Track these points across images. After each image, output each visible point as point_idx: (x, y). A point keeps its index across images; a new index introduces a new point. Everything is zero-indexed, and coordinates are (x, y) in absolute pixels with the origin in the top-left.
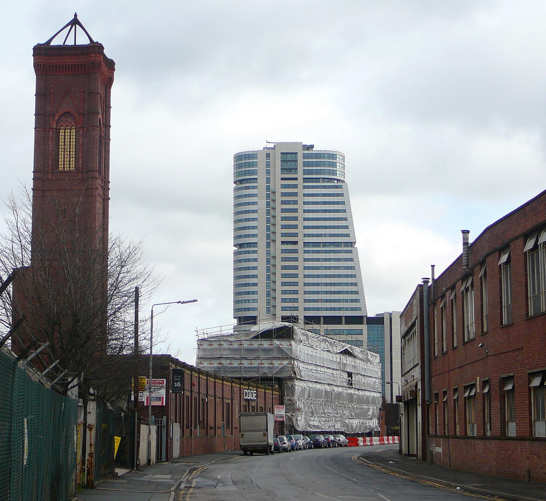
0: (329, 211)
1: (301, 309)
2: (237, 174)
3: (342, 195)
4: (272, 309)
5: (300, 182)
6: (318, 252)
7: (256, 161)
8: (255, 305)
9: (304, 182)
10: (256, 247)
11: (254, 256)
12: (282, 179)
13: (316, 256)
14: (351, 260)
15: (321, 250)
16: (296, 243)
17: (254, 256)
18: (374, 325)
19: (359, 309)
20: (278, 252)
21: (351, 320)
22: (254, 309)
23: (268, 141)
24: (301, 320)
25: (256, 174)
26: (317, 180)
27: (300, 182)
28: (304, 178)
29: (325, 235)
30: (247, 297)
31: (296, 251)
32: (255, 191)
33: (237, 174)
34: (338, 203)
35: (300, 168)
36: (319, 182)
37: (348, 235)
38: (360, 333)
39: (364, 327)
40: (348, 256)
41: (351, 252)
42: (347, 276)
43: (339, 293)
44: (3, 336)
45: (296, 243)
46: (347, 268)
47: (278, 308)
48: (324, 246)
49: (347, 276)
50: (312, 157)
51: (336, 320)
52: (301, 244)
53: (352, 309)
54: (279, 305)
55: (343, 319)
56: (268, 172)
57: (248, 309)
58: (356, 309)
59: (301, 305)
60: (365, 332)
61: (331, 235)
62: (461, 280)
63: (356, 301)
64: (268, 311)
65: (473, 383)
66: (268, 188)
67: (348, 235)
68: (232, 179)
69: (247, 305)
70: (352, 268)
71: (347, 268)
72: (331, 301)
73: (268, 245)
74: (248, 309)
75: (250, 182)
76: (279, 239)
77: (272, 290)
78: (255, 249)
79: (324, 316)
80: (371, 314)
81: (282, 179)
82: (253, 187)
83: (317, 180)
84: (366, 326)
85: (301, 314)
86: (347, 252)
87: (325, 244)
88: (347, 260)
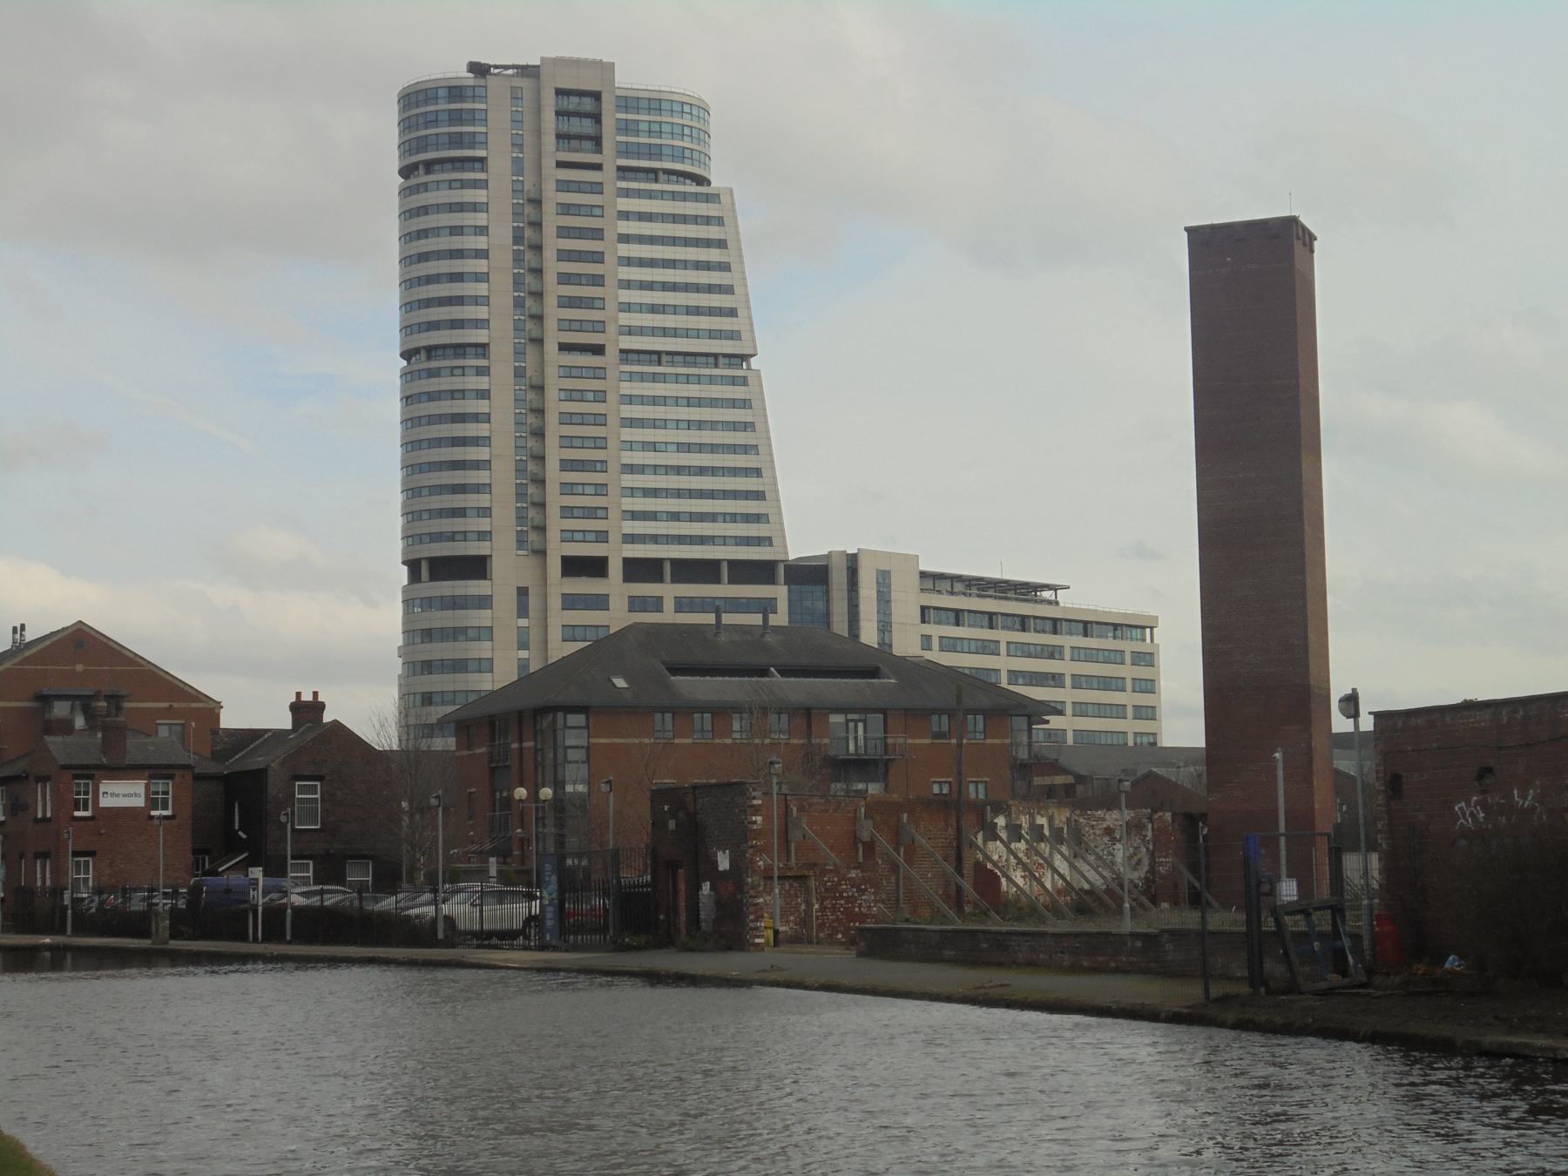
0: (714, 471)
2: (407, 147)
3: (728, 290)
9: (619, 178)
12: (560, 165)
13: (659, 389)
17: (479, 195)
24: (615, 569)
26: (653, 174)
27: (607, 176)
28: (620, 169)
29: (675, 310)
32: (479, 195)
33: (408, 146)
34: (707, 243)
37: (734, 335)
40: (737, 392)
41: (744, 381)
45: (598, 350)
46: (734, 426)
47: (553, 535)
54: (555, 524)
61: (689, 402)
63: (757, 518)
64: (521, 542)
67: (734, 335)
68: (394, 164)
70: (747, 426)
71: (734, 426)
72: (651, 263)
73: (519, 353)
76: (553, 338)
77: (532, 481)
78: (482, 362)
80: (799, 546)
81: (560, 165)
82: (475, 184)
83: (653, 174)
84: (786, 587)
85: (617, 553)
86: (734, 381)
88: (733, 403)
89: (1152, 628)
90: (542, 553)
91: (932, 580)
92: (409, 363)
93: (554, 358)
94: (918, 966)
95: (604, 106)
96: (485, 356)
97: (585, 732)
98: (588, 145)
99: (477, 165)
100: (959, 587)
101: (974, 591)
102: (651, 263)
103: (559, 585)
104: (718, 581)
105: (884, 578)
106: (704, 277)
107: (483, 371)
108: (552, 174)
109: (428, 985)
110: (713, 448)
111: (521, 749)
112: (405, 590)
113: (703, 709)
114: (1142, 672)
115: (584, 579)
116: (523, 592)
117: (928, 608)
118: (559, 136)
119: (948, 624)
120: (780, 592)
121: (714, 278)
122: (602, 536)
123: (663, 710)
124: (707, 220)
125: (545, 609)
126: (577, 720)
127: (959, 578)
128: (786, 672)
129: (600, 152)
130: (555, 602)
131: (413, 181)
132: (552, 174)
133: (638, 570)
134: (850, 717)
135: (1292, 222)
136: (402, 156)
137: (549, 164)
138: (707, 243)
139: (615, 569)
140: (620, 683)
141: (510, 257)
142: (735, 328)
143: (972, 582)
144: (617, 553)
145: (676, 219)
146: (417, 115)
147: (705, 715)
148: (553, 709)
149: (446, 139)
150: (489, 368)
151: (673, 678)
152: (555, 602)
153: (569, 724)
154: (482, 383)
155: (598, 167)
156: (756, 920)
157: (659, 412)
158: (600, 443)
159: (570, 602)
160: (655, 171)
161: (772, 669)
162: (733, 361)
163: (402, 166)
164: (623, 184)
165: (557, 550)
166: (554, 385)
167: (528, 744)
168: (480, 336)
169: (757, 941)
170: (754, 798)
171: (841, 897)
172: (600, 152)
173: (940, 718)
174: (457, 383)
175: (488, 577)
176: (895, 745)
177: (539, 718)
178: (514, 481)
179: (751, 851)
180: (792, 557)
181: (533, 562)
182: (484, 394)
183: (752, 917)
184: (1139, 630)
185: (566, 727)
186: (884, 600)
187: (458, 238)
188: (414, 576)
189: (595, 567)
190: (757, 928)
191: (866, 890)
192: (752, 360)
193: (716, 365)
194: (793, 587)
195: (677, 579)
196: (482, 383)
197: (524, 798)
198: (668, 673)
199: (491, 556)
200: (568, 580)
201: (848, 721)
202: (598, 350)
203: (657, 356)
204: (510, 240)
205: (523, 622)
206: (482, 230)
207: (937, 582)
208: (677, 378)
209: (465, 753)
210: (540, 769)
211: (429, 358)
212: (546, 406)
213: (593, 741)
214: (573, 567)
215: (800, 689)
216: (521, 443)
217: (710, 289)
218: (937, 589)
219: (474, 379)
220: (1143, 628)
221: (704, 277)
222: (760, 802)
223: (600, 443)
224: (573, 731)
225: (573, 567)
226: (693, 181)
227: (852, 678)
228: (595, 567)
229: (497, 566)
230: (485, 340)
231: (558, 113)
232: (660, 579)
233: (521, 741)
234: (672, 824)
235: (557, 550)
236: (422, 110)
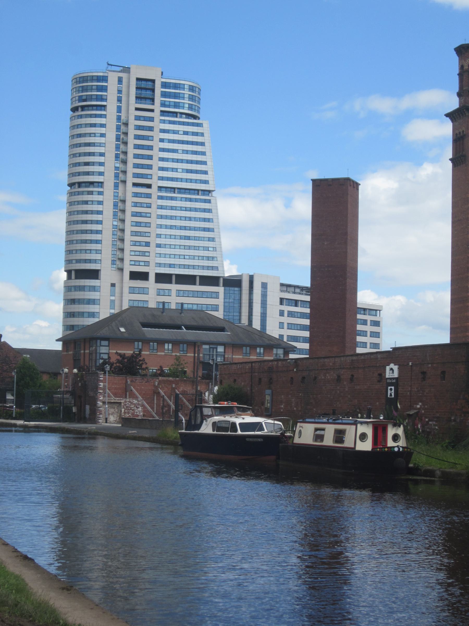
5: (156, 115)
7: (106, 84)
8: (98, 257)
9: (161, 115)
10: (102, 187)
11: (103, 121)
12: (137, 109)
14: (209, 211)
15: (199, 237)
17: (103, 121)
18: (231, 288)
19: (216, 268)
22: (95, 261)
23: (109, 63)
24: (152, 277)
25: (106, 100)
26: (175, 114)
27: (156, 115)
28: (162, 111)
30: (88, 246)
31: (149, 196)
34: (197, 143)
35: (158, 98)
36: (177, 117)
38: (216, 295)
39: (221, 290)
40: (206, 206)
42: (205, 230)
45: (149, 186)
49: (205, 230)
50: (170, 87)
53: (208, 268)
54: (127, 257)
55: (198, 279)
56: (119, 100)
57: (90, 261)
58: (213, 268)
59: (153, 259)
60: (221, 295)
66: (119, 118)
69: (88, 256)
73: (116, 186)
74: (90, 261)
75: (93, 110)
76: (130, 180)
78: (100, 190)
81: (137, 109)
82: (101, 116)
84: (223, 288)
85: (152, 271)
87: (181, 190)
88: (205, 210)
89: (380, 311)
90: (121, 270)
91: (285, 287)
92: (71, 188)
93: (130, 189)
95: (156, 85)
96: (102, 187)
97: (108, 348)
98: (148, 101)
99: (103, 108)
100: (298, 290)
101: (304, 292)
103: (128, 283)
104: (194, 284)
105: (264, 286)
106: (188, 233)
107: (100, 193)
108: (130, 189)
109: (282, 504)
111: (84, 353)
112: (65, 282)
113: (154, 341)
114: (375, 329)
115: (139, 281)
116: (113, 285)
117: (284, 299)
118: (137, 98)
119: (292, 306)
122: (147, 264)
123: (138, 341)
125: (122, 293)
126: (105, 343)
127: (298, 287)
128: (188, 328)
129: (153, 104)
130: (126, 290)
131: (77, 114)
133: (161, 278)
134: (211, 346)
135: (348, 180)
136: (72, 103)
137: (132, 108)
138: (197, 143)
139: (152, 277)
140: (122, 330)
141: (114, 146)
142: (207, 179)
143: (304, 289)
144: (152, 271)
146: (79, 87)
147: (155, 343)
148: (96, 339)
150: (103, 192)
151: (143, 329)
152: (126, 290)
153: (102, 344)
154: (100, 198)
155: (152, 111)
156: (99, 415)
157: (173, 213)
158: (148, 225)
159: (132, 290)
160: (176, 113)
161: (183, 327)
162: (206, 193)
163: (72, 107)
164: (163, 118)
166: (130, 200)
167: (87, 351)
168: (100, 179)
169: (99, 421)
170: (101, 377)
171: (131, 409)
172: (153, 104)
173: (246, 349)
174: (89, 198)
175: (99, 279)
176: (228, 358)
177: (91, 341)
178: (111, 239)
179: (99, 394)
180: (226, 275)
182: (100, 203)
183: (98, 414)
184: (374, 311)
185: (101, 346)
186: (264, 296)
187: (91, 196)
188: (69, 277)
189: (144, 276)
190: (100, 417)
191: (139, 407)
192: (213, 193)
193: (198, 194)
194: (227, 288)
195: (177, 283)
196: (100, 198)
197: (67, 372)
198: (141, 327)
199: (100, 270)
200: (132, 281)
201: (210, 348)
202: (149, 186)
203: (173, 189)
204: (115, 140)
205: (113, 298)
206: (102, 155)
207: (288, 288)
208: (181, 199)
209: (66, 353)
210: (91, 361)
211: (79, 187)
212: (126, 208)
213: (111, 351)
214: (135, 276)
215: (192, 335)
217: (197, 162)
218: (288, 291)
219: (97, 196)
220: (376, 310)
221: (188, 233)
222: (102, 379)
223: (148, 225)
224: (104, 347)
225: (135, 276)
226: (192, 117)
227: (206, 331)
228: (144, 276)
229: (103, 274)
230: (102, 180)
231: (137, 88)
232: (170, 282)
233: (84, 350)
234: (80, 384)
236: (81, 85)
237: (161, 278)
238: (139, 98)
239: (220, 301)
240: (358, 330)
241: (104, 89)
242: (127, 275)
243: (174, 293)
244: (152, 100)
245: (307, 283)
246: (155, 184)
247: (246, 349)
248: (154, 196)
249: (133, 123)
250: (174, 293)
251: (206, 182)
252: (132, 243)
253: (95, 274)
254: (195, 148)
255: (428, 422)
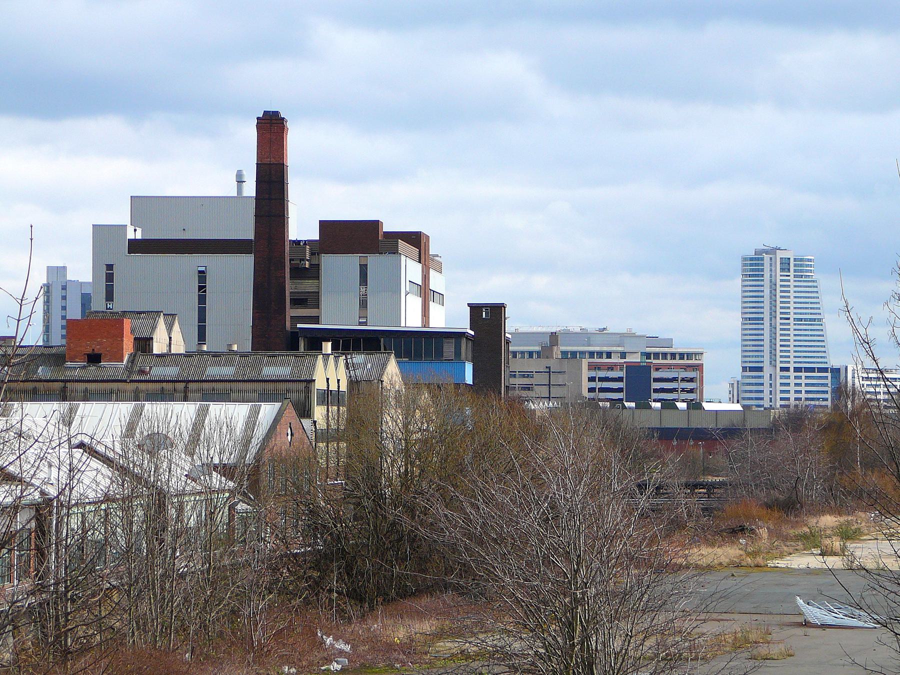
0: (801, 297)
1: (792, 362)
4: (773, 362)
6: (801, 324)
9: (794, 278)
12: (781, 276)
16: (788, 319)
20: (778, 324)
21: (821, 370)
24: (792, 370)
27: (792, 278)
35: (792, 269)
38: (826, 378)
43: (818, 352)
44: (73, 438)
46: (819, 336)
47: (778, 362)
48: (810, 321)
51: (812, 370)
52: (792, 319)
54: (778, 359)
60: (830, 378)
62: (302, 420)
65: (763, 389)
66: (771, 281)
72: (808, 292)
73: (771, 320)
79: (804, 368)
81: (781, 276)
85: (792, 366)
87: (806, 320)
94: (275, 415)
102: (814, 352)
106: (812, 311)
110: (801, 303)
116: (771, 375)
120: (829, 375)
121: (817, 311)
122: (789, 362)
124: (814, 287)
132: (779, 278)
133: (797, 370)
139: (792, 370)
145: (806, 287)
149: (749, 270)
152: (778, 377)
155: (789, 276)
165: (779, 365)
173: (339, 387)
181: (773, 367)
189: (787, 369)
205: (771, 382)
214: (782, 369)
216: (307, 285)
225: (782, 369)
228: (787, 369)
235: (779, 365)
237: (797, 370)
238: (782, 270)
239: (829, 381)
240: (83, 311)
241: (763, 265)
242: (778, 369)
243: (803, 378)
244: (789, 270)
245: (136, 238)
246: (792, 316)
247: (339, 387)
248: (792, 324)
249: (779, 283)
250: (803, 378)
251: (820, 314)
252: (762, 377)
253: (760, 369)
254: (800, 289)
255: (15, 550)
